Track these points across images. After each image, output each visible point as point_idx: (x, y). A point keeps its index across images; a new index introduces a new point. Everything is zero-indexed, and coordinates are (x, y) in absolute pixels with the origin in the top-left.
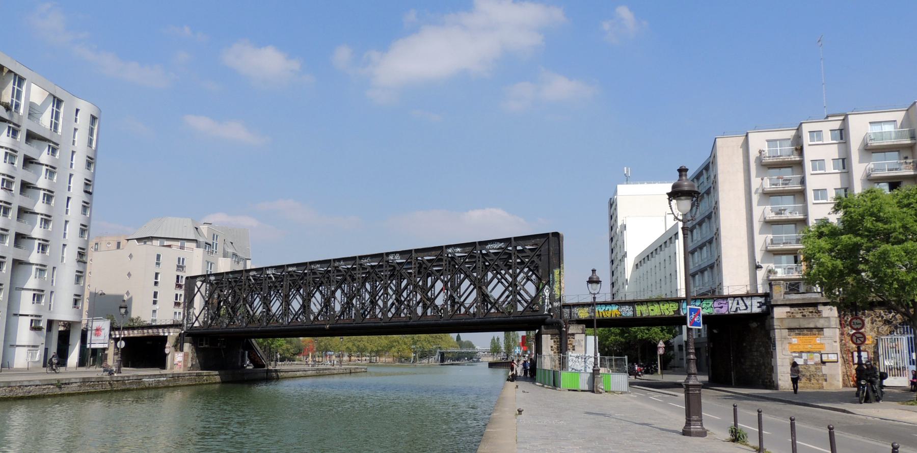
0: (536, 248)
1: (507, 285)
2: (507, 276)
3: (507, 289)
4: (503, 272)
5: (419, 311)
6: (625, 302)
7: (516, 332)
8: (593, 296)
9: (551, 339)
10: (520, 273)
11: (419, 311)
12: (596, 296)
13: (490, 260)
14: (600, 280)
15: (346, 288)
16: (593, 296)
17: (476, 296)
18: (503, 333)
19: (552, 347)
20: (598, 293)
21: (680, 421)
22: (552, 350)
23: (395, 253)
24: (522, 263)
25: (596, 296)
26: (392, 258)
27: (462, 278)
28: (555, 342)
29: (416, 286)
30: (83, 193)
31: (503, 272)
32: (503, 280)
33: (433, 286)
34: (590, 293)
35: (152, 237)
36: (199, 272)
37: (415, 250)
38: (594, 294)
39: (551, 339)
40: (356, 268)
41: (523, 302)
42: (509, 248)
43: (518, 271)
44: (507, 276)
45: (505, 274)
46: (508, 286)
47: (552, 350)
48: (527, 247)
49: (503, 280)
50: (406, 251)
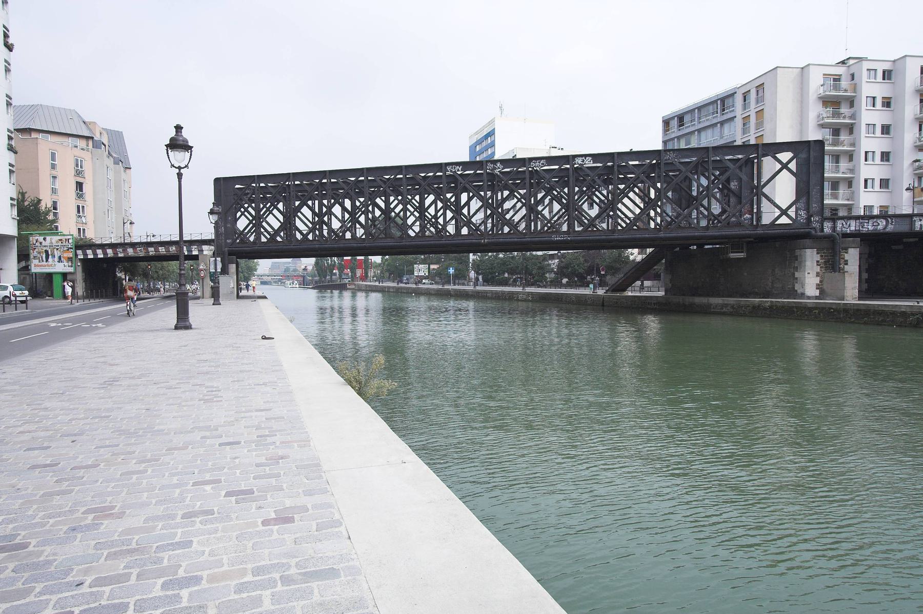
0: (278, 186)
1: (251, 218)
2: (250, 209)
3: (251, 222)
4: (246, 206)
5: (451, 229)
6: (917, 216)
7: (255, 260)
8: (177, 171)
9: (818, 253)
10: (263, 208)
11: (451, 229)
12: (182, 171)
13: (584, 175)
14: (190, 144)
15: (348, 203)
16: (177, 171)
17: (297, 225)
18: (637, 249)
19: (818, 262)
20: (186, 166)
21: (174, 321)
22: (818, 265)
23: (586, 156)
24: (265, 198)
25: (182, 171)
26: (580, 162)
27: (332, 202)
28: (821, 256)
29: (445, 201)
30: (10, 36)
31: (246, 206)
32: (246, 213)
33: (467, 204)
34: (173, 166)
35: (29, 129)
36: (785, 135)
37: (713, 147)
38: (180, 168)
39: (818, 253)
40: (441, 176)
41: (265, 233)
42: (252, 185)
43: (262, 206)
44: (250, 209)
45: (248, 207)
46: (252, 220)
47: (818, 265)
48: (269, 185)
49: (246, 213)
50: (559, 156)
